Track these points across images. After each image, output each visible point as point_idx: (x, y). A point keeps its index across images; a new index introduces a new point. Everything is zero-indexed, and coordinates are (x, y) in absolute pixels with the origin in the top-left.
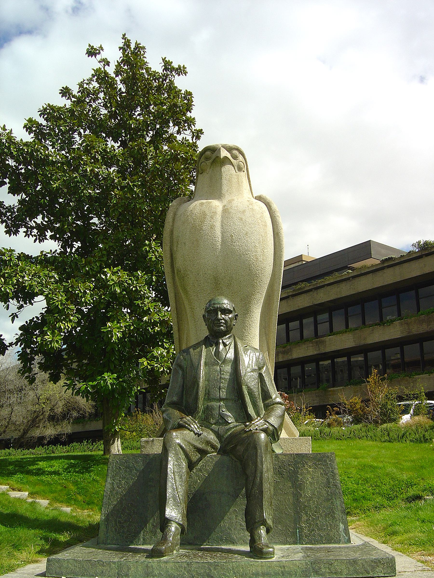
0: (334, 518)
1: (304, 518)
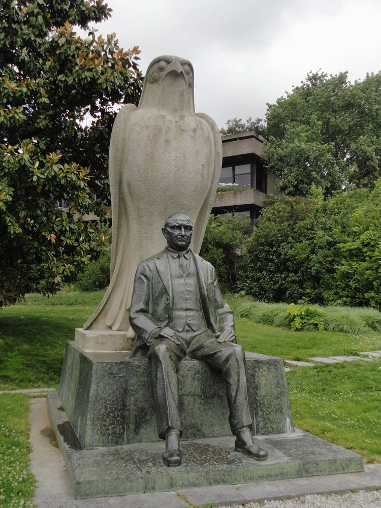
0: (282, 413)
1: (260, 413)
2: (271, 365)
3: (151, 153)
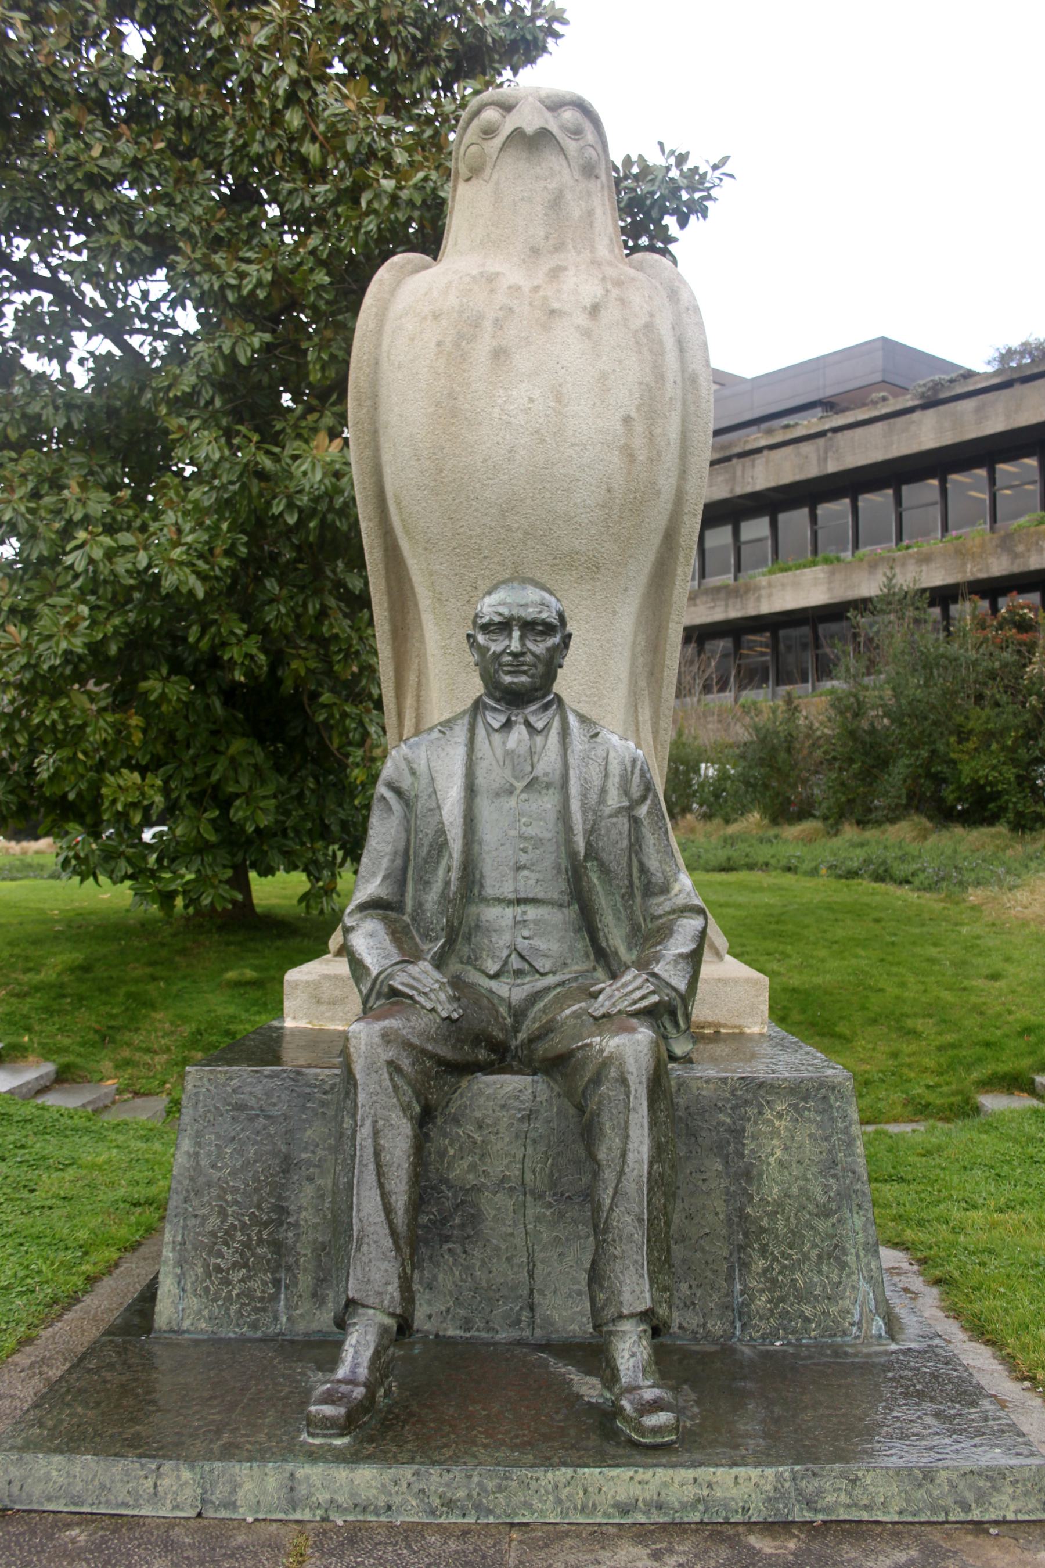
0: (843, 1265)
1: (760, 1264)
2: (805, 1099)
3: (450, 394)
